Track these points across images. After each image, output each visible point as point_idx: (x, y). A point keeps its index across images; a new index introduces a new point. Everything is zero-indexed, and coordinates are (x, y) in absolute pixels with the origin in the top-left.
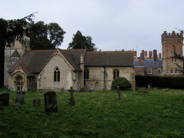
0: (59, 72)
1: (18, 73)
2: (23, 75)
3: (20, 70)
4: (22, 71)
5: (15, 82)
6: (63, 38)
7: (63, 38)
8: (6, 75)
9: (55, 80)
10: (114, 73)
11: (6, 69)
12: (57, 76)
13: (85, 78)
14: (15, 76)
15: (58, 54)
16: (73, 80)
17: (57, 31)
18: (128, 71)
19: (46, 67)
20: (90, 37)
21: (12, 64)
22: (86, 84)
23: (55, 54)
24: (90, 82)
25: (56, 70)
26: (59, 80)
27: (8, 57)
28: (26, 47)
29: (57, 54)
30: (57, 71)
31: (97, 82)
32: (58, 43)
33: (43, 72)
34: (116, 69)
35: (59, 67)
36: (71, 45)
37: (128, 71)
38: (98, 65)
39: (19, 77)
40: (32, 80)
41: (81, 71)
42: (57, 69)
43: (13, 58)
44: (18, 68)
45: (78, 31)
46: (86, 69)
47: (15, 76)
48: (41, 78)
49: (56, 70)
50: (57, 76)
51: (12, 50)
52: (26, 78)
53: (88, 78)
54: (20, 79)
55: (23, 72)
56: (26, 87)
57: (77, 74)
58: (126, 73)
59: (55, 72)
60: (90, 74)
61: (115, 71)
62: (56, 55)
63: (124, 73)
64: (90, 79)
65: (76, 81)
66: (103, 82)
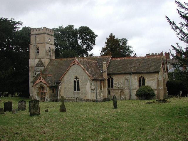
0: (78, 82)
1: (40, 83)
2: (45, 86)
3: (41, 81)
4: (44, 81)
5: (38, 92)
6: (110, 36)
7: (110, 36)
8: (31, 84)
9: (75, 90)
10: (140, 81)
11: (31, 79)
12: (77, 86)
13: (109, 86)
14: (37, 86)
15: (77, 63)
16: (92, 89)
17: (87, 34)
18: (153, 78)
19: (66, 76)
20: (125, 39)
21: (36, 74)
22: (111, 93)
23: (74, 63)
24: (115, 91)
25: (76, 80)
26: (79, 90)
27: (32, 67)
28: (51, 56)
29: (75, 63)
30: (76, 81)
31: (122, 91)
32: (90, 48)
33: (64, 82)
34: (142, 76)
35: (78, 77)
36: (104, 50)
37: (153, 78)
38: (128, 71)
39: (41, 88)
40: (55, 91)
41: (104, 80)
42: (76, 78)
43: (37, 67)
44: (40, 78)
45: (111, 34)
46: (110, 77)
47: (37, 86)
48: (61, 88)
49: (76, 80)
50: (77, 86)
51: (36, 60)
52: (48, 88)
53: (112, 86)
54: (42, 88)
55: (44, 82)
56: (48, 97)
57: (98, 83)
58: (153, 80)
59: (75, 82)
60: (114, 82)
61: (140, 78)
62: (75, 65)
63: (150, 80)
64: (114, 88)
65: (95, 91)
66: (128, 91)
